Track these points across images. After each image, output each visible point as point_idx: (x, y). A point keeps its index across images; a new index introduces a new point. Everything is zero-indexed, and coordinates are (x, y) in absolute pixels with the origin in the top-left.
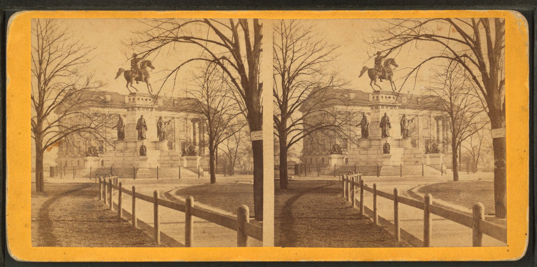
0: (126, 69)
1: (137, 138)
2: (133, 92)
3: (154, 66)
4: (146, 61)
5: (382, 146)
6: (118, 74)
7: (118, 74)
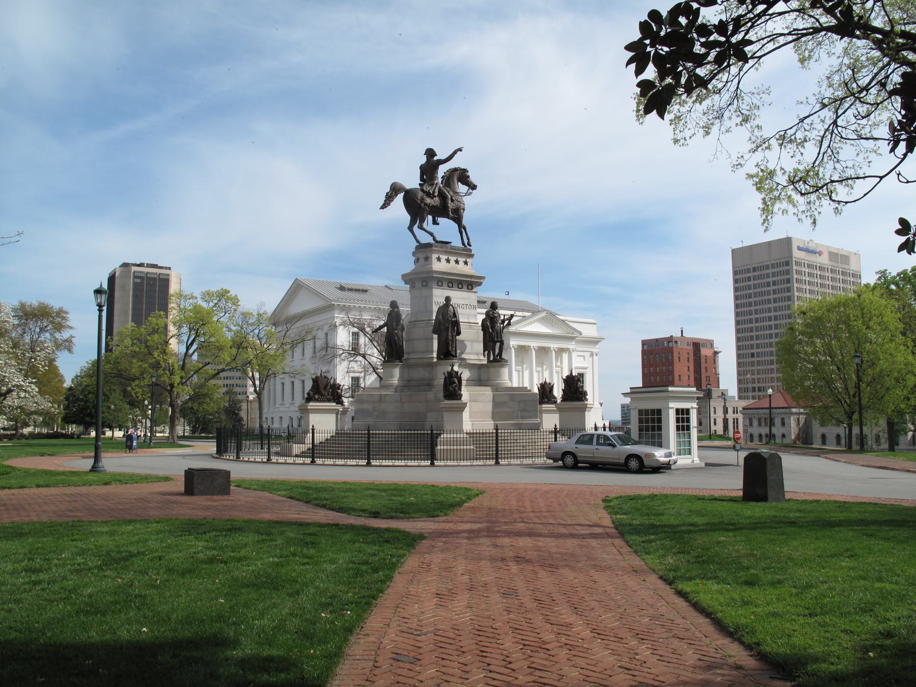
0: (408, 186)
1: (435, 355)
2: (423, 241)
3: (475, 182)
4: (456, 170)
5: (440, 381)
6: (389, 198)
7: (389, 198)
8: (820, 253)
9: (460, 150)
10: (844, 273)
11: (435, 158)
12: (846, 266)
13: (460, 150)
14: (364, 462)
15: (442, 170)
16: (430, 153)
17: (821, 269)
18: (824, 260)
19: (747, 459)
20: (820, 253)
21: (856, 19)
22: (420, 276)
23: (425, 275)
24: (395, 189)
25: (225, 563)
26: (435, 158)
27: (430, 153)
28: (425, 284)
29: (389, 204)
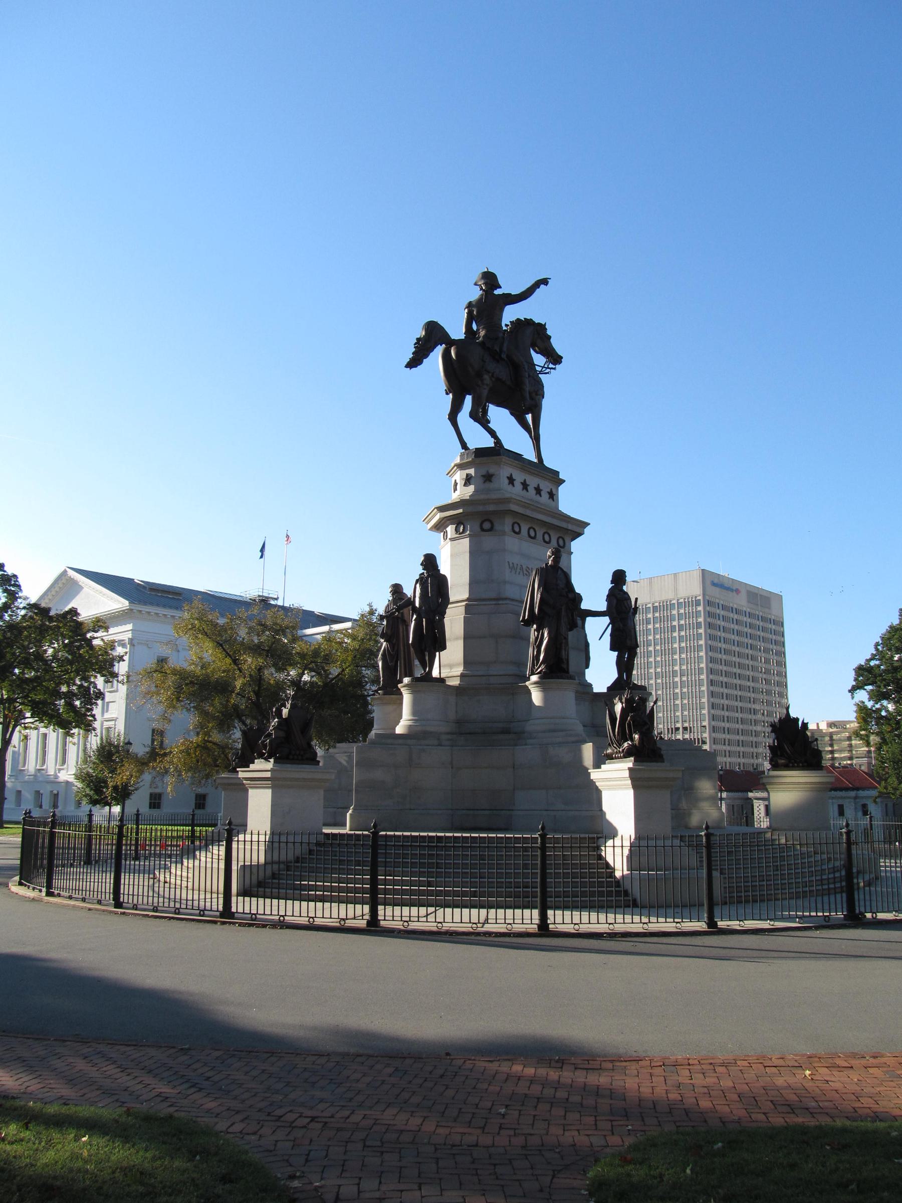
4: (529, 322)
8: (737, 591)
9: (545, 282)
10: (763, 619)
11: (497, 292)
12: (767, 610)
13: (545, 282)
14: (356, 913)
15: (510, 315)
16: (490, 280)
17: (737, 612)
18: (741, 602)
19: (370, 725)
20: (737, 591)
21: (471, 489)
22: (481, 508)
23: (491, 508)
24: (433, 335)
25: (132, 776)
26: (497, 292)
27: (490, 280)
28: (487, 525)
29: (420, 363)
